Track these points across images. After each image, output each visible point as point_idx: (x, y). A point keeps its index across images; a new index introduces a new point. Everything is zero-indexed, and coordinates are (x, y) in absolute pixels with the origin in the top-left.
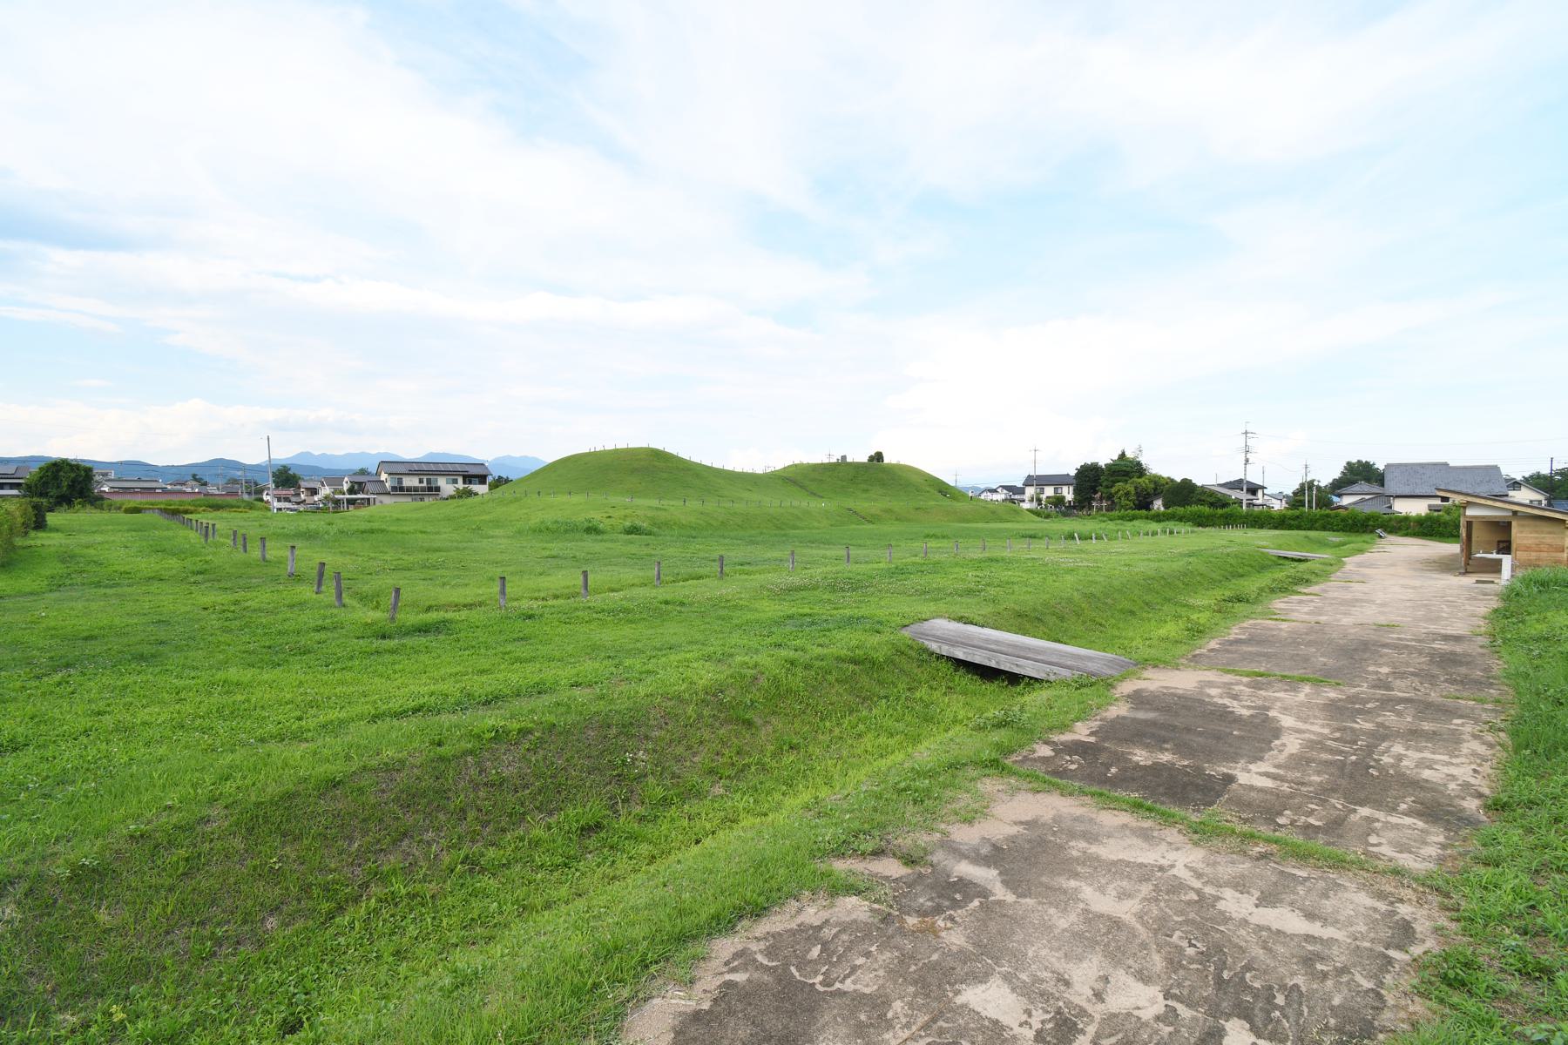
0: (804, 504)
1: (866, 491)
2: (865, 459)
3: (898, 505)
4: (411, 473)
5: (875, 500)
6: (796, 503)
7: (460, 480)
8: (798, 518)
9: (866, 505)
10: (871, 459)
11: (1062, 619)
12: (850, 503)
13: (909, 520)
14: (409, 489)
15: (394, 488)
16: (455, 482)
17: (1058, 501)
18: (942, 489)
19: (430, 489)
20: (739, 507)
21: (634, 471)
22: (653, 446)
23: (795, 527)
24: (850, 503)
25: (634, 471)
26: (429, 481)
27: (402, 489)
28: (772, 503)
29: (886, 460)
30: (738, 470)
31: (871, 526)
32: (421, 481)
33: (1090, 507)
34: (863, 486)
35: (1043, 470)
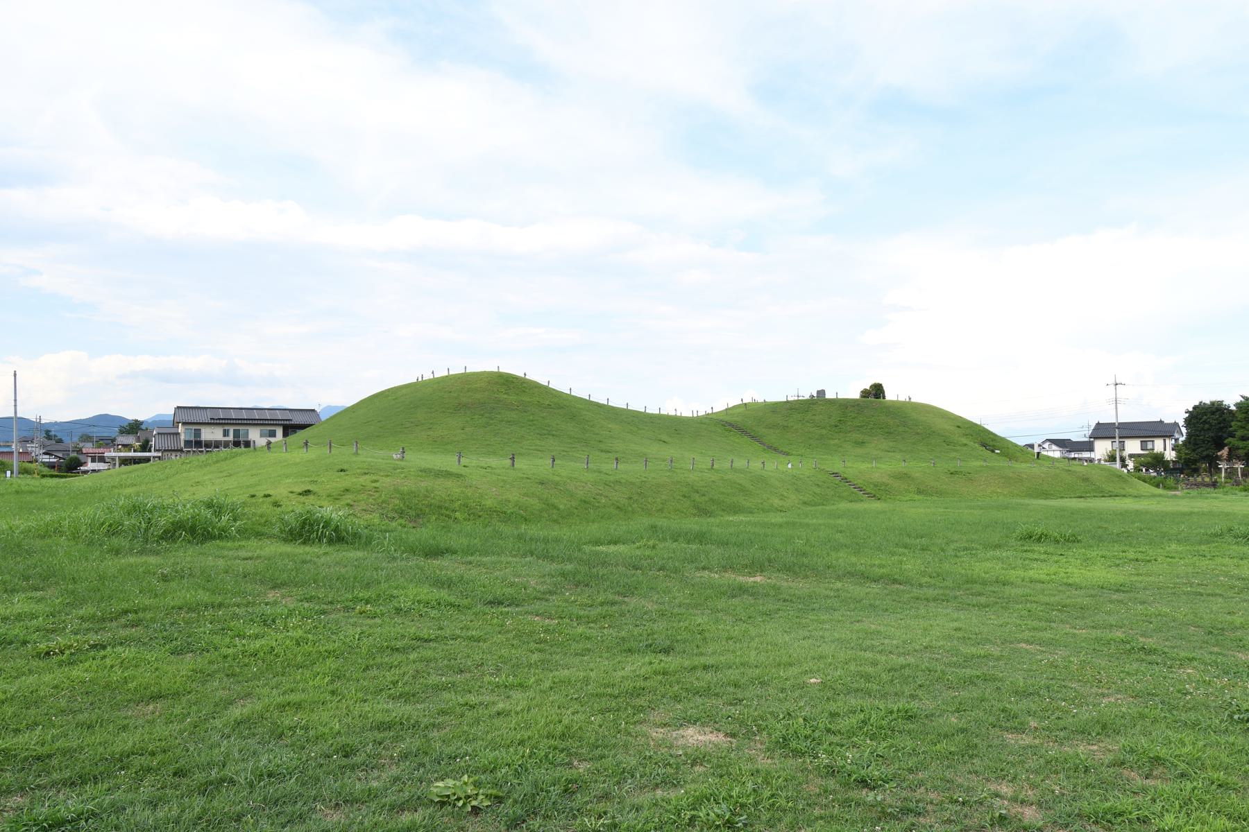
0: (756, 465)
1: (861, 444)
2: (856, 395)
3: (918, 467)
4: (214, 423)
5: (877, 459)
6: (740, 463)
7: (279, 432)
8: (743, 491)
9: (864, 466)
10: (865, 394)
11: (808, 805)
12: (836, 464)
13: (940, 493)
14: (208, 445)
15: (188, 443)
16: (273, 434)
17: (1157, 461)
18: (988, 442)
19: (237, 444)
20: (631, 470)
21: (460, 407)
22: (505, 369)
23: (735, 509)
24: (835, 464)
25: (460, 407)
26: (236, 433)
27: (198, 444)
28: (696, 464)
29: (890, 395)
30: (652, 410)
31: (876, 505)
32: (226, 433)
33: (1214, 468)
34: (857, 436)
35: (1129, 415)
